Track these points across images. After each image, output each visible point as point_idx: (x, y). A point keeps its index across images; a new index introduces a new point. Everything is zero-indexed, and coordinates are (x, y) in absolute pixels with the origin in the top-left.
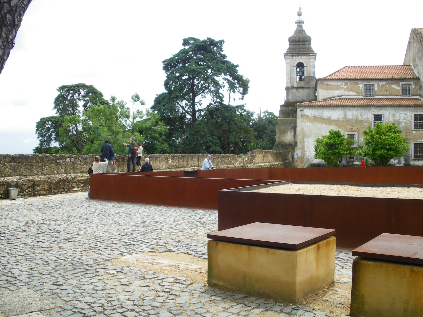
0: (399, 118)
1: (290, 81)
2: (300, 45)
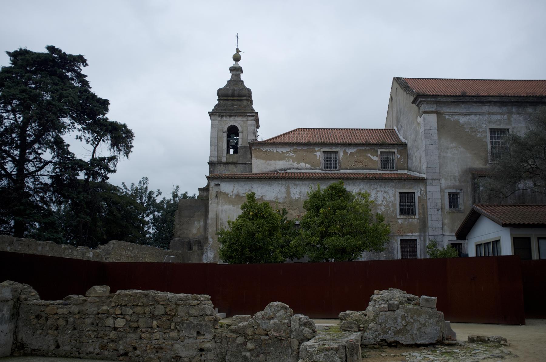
0: (376, 199)
2: (234, 101)
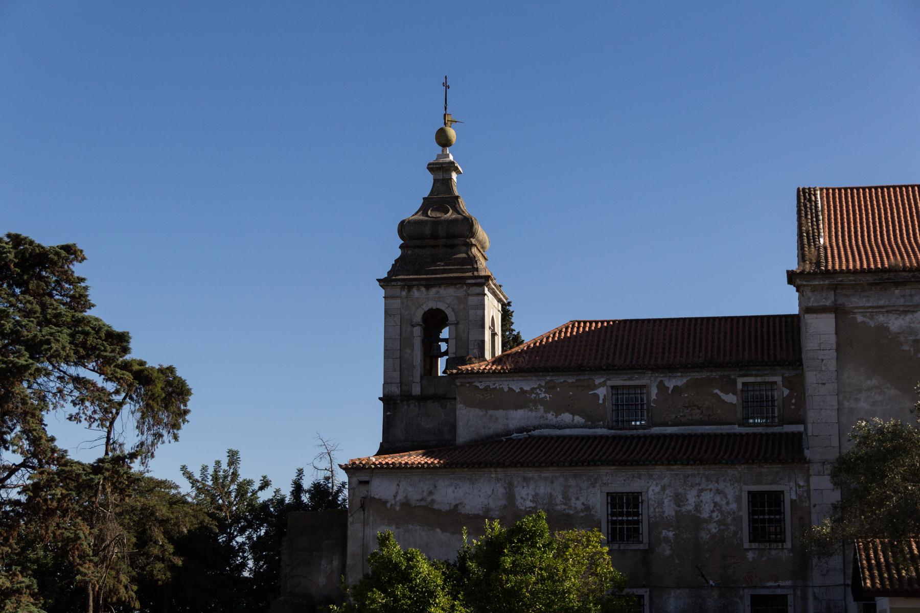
0: (698, 507)
1: (397, 375)
